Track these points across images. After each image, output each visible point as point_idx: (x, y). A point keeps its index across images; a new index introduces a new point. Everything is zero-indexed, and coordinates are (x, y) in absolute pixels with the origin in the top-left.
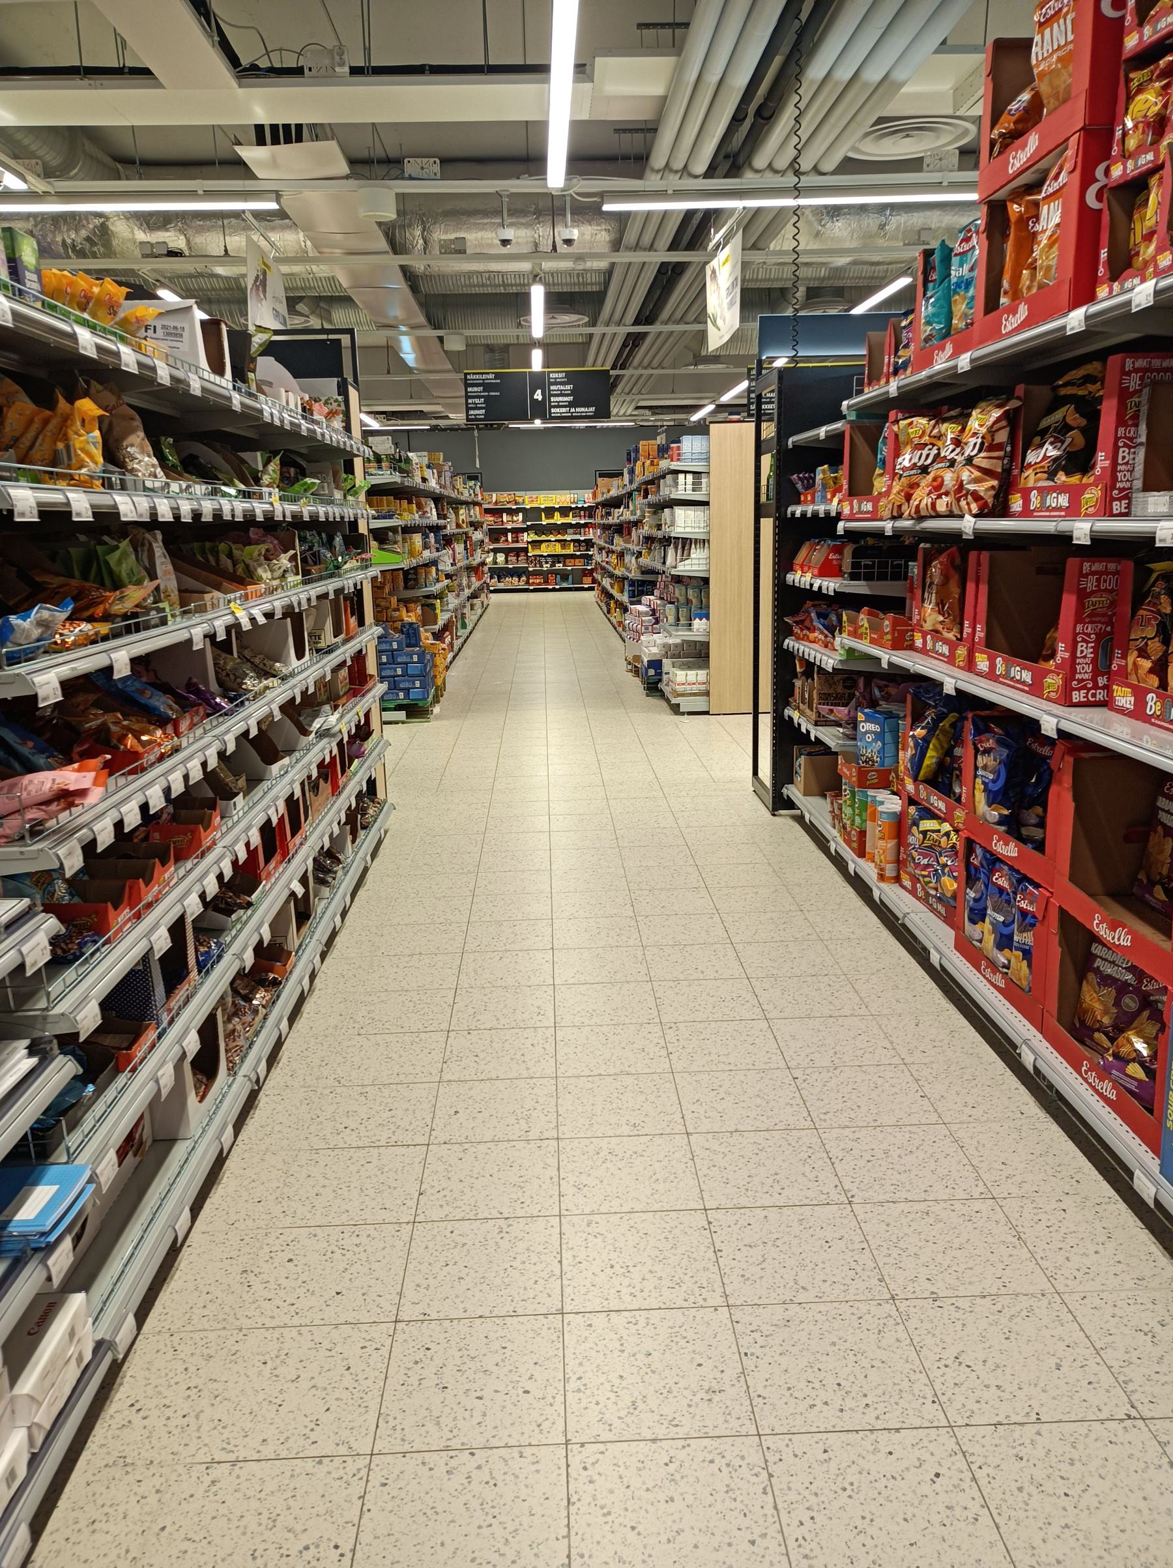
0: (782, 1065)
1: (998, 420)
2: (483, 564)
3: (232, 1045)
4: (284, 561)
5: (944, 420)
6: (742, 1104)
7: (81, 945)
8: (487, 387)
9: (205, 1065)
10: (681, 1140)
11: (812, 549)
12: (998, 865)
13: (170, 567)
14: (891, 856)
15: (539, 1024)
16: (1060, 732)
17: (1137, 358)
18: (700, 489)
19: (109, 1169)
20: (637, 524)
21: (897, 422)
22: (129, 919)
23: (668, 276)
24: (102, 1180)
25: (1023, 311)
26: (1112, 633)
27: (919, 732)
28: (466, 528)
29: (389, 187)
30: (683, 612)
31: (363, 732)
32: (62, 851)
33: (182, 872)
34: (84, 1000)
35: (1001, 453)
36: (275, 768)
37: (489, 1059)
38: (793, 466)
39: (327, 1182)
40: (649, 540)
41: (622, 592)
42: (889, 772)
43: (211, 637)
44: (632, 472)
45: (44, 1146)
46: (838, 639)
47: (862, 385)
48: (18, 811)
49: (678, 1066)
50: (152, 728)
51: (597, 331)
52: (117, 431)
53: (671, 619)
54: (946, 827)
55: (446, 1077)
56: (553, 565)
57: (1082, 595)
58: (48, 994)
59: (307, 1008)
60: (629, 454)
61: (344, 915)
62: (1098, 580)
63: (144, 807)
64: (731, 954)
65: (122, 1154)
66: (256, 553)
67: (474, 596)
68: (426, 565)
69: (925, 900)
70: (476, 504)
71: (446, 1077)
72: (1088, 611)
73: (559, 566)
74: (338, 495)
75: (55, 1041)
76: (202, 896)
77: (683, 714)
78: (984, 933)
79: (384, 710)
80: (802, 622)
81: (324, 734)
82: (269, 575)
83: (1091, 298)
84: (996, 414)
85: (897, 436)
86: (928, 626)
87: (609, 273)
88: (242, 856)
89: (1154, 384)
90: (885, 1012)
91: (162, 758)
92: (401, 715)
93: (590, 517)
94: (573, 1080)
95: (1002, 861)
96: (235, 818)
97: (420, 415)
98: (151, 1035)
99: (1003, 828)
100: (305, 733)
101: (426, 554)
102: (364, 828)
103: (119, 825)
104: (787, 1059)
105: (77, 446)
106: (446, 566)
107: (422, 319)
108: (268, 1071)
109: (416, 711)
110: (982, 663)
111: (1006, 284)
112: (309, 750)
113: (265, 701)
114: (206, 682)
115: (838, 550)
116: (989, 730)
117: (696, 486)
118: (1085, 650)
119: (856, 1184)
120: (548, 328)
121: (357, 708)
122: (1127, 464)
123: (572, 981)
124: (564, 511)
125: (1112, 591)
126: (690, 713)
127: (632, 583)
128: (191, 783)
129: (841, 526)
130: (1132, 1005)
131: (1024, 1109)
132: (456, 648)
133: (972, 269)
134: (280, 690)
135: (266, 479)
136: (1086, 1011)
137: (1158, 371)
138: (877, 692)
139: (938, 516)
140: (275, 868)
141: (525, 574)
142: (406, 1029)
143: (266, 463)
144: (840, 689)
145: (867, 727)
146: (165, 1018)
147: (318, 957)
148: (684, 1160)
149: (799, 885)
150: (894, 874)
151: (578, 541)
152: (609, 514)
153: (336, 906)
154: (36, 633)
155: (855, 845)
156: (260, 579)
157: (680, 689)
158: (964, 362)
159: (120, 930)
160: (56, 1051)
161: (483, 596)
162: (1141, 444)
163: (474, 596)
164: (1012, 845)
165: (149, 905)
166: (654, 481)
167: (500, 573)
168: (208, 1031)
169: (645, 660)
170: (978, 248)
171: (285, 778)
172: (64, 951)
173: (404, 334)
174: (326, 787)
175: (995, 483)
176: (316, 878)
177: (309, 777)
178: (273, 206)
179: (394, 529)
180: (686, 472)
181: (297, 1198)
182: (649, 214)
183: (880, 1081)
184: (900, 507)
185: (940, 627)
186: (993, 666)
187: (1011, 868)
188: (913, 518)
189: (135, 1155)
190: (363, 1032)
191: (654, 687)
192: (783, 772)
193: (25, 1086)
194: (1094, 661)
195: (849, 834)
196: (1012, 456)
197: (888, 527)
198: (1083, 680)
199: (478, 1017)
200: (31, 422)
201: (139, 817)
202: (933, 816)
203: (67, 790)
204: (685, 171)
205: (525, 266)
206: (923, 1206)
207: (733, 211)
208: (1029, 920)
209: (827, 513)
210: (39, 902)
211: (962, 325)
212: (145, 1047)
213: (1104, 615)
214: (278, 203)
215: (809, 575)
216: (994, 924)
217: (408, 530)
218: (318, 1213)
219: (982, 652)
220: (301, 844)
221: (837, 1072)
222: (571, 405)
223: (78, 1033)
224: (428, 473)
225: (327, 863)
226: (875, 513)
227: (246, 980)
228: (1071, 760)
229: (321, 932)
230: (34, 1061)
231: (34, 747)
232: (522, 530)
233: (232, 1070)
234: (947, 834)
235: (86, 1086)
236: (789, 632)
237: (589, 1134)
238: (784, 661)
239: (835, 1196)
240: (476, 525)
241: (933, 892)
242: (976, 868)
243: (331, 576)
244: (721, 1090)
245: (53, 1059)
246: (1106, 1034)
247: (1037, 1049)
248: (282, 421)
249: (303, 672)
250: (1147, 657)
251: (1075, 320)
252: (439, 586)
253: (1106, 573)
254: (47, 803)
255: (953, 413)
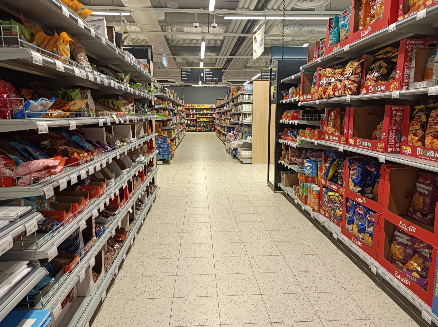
0: (290, 271)
1: (357, 66)
2: (184, 123)
3: (106, 262)
4: (130, 106)
5: (336, 69)
6: (278, 284)
7: (52, 226)
8: (188, 72)
9: (97, 270)
10: (259, 297)
11: (288, 113)
12: (358, 206)
13: (93, 101)
14: (317, 204)
15: (208, 256)
16: (386, 161)
17: (411, 40)
18: (250, 99)
19: (57, 311)
20: (231, 110)
21: (320, 70)
22: (72, 217)
23: (241, 40)
24: (55, 315)
25: (369, 29)
26: (401, 129)
27: (327, 165)
28: (180, 112)
29: (163, 10)
30: (244, 135)
31: (151, 164)
32: (45, 189)
33: (92, 202)
34: (52, 245)
35: (358, 76)
36: (125, 171)
37: (192, 267)
38: (283, 88)
39: (138, 312)
40: (234, 115)
41: (224, 131)
42: (315, 178)
43: (105, 124)
44: (228, 97)
45: (33, 302)
46: (298, 138)
47: (306, 62)
48: (29, 174)
49: (255, 271)
50: (84, 152)
51: (219, 57)
52: (76, 51)
53: (241, 137)
54: (337, 194)
55: (178, 274)
56: (204, 124)
57: (391, 117)
58: (37, 244)
59: (132, 250)
60: (227, 92)
61: (144, 220)
62: (396, 112)
63: (79, 177)
64: (268, 234)
65: (63, 305)
66: (121, 103)
67: (181, 131)
68: (169, 120)
69: (329, 218)
70: (183, 106)
71: (178, 274)
72: (393, 122)
73: (205, 124)
74: (146, 91)
75: (39, 262)
76: (99, 210)
77: (244, 164)
78: (354, 228)
79: (158, 161)
80: (285, 134)
81: (140, 162)
82: (125, 110)
83: (396, 20)
84: (357, 64)
85: (320, 74)
86: (330, 132)
87: (223, 41)
88: (113, 198)
89: (418, 48)
90: (320, 253)
91: (86, 162)
92: (161, 162)
93: (214, 111)
94: (221, 275)
95: (359, 204)
96: (111, 186)
97: (167, 82)
98: (78, 259)
99: (359, 194)
100: (134, 161)
101: (169, 117)
102: (151, 194)
103: (69, 182)
104: (291, 269)
105: (61, 49)
106: (174, 121)
107: (169, 52)
108: (119, 271)
109: (165, 161)
110: (352, 141)
111: (361, 22)
112: (135, 167)
113: (121, 150)
114: (103, 141)
115: (297, 112)
116: (354, 163)
117: (249, 98)
118: (392, 135)
119: (322, 314)
120: (205, 56)
121: (150, 156)
122: (407, 74)
123: (217, 242)
124: (207, 109)
125: (401, 116)
126: (246, 164)
127: (228, 128)
128: (96, 171)
129: (300, 104)
130: (410, 252)
131: (372, 287)
132: (177, 145)
133: (348, 21)
134: (127, 146)
135: (125, 80)
136: (393, 254)
137: (418, 45)
138: (309, 155)
139: (336, 97)
140: (123, 203)
141: (196, 127)
142: (165, 257)
143: (125, 76)
144: (297, 154)
145: (307, 164)
146: (83, 253)
147: (136, 233)
148: (262, 304)
149: (286, 213)
150: (318, 210)
151: (211, 118)
152: (220, 109)
153: (142, 217)
154: (40, 108)
155: (304, 201)
156: (122, 111)
157: (243, 156)
158: (346, 48)
159: (68, 221)
160: (39, 265)
161: (184, 132)
162: (413, 67)
163: (181, 131)
164: (364, 199)
165: (79, 213)
166: (236, 98)
167: (189, 126)
168: (98, 258)
169: (233, 149)
170: (351, 14)
171: (127, 175)
172: (46, 228)
173: (164, 56)
174: (140, 179)
175: (357, 85)
176: (136, 208)
177: (135, 175)
178: (129, 14)
179: (160, 108)
180: (246, 94)
181: (127, 317)
182: (237, 20)
183: (323, 277)
184: (321, 95)
185: (334, 132)
186: (356, 142)
187: (364, 207)
188: (327, 98)
189: (70, 302)
190: (150, 258)
191: (235, 156)
192: (278, 179)
193: (27, 277)
194: (395, 139)
195: (302, 197)
196: (362, 77)
197: (317, 102)
198: (391, 145)
199: (188, 253)
200: (45, 40)
201: (77, 180)
202: (332, 191)
203: (49, 166)
204: (248, 8)
205: (199, 37)
206: (346, 322)
207: (261, 20)
208: (371, 223)
209: (295, 101)
210: (35, 208)
211: (344, 38)
212: (75, 264)
213: (398, 124)
214: (130, 13)
215: (288, 120)
216: (358, 225)
217: (164, 109)
218: (135, 323)
219: (351, 138)
220: (132, 196)
221: (308, 273)
222: (211, 77)
223: (48, 259)
224: (170, 94)
225: (140, 203)
226: (313, 98)
227: (112, 240)
228: (389, 170)
229: (137, 225)
230: (30, 269)
231: (39, 154)
232: (195, 114)
233: (106, 271)
234: (338, 197)
235: (51, 278)
236: (281, 138)
237: (228, 294)
238: (278, 146)
239: (315, 318)
240: (183, 112)
241: (333, 215)
242: (349, 207)
243: (144, 115)
244: (271, 279)
245: (37, 269)
246: (401, 262)
247: (376, 267)
248: (131, 63)
249: (134, 142)
250: (417, 136)
251: (392, 27)
252: (173, 127)
253: (399, 110)
254: (41, 171)
255: (338, 67)
